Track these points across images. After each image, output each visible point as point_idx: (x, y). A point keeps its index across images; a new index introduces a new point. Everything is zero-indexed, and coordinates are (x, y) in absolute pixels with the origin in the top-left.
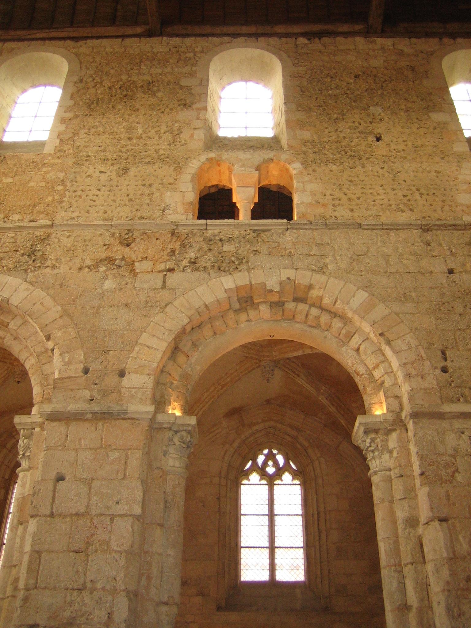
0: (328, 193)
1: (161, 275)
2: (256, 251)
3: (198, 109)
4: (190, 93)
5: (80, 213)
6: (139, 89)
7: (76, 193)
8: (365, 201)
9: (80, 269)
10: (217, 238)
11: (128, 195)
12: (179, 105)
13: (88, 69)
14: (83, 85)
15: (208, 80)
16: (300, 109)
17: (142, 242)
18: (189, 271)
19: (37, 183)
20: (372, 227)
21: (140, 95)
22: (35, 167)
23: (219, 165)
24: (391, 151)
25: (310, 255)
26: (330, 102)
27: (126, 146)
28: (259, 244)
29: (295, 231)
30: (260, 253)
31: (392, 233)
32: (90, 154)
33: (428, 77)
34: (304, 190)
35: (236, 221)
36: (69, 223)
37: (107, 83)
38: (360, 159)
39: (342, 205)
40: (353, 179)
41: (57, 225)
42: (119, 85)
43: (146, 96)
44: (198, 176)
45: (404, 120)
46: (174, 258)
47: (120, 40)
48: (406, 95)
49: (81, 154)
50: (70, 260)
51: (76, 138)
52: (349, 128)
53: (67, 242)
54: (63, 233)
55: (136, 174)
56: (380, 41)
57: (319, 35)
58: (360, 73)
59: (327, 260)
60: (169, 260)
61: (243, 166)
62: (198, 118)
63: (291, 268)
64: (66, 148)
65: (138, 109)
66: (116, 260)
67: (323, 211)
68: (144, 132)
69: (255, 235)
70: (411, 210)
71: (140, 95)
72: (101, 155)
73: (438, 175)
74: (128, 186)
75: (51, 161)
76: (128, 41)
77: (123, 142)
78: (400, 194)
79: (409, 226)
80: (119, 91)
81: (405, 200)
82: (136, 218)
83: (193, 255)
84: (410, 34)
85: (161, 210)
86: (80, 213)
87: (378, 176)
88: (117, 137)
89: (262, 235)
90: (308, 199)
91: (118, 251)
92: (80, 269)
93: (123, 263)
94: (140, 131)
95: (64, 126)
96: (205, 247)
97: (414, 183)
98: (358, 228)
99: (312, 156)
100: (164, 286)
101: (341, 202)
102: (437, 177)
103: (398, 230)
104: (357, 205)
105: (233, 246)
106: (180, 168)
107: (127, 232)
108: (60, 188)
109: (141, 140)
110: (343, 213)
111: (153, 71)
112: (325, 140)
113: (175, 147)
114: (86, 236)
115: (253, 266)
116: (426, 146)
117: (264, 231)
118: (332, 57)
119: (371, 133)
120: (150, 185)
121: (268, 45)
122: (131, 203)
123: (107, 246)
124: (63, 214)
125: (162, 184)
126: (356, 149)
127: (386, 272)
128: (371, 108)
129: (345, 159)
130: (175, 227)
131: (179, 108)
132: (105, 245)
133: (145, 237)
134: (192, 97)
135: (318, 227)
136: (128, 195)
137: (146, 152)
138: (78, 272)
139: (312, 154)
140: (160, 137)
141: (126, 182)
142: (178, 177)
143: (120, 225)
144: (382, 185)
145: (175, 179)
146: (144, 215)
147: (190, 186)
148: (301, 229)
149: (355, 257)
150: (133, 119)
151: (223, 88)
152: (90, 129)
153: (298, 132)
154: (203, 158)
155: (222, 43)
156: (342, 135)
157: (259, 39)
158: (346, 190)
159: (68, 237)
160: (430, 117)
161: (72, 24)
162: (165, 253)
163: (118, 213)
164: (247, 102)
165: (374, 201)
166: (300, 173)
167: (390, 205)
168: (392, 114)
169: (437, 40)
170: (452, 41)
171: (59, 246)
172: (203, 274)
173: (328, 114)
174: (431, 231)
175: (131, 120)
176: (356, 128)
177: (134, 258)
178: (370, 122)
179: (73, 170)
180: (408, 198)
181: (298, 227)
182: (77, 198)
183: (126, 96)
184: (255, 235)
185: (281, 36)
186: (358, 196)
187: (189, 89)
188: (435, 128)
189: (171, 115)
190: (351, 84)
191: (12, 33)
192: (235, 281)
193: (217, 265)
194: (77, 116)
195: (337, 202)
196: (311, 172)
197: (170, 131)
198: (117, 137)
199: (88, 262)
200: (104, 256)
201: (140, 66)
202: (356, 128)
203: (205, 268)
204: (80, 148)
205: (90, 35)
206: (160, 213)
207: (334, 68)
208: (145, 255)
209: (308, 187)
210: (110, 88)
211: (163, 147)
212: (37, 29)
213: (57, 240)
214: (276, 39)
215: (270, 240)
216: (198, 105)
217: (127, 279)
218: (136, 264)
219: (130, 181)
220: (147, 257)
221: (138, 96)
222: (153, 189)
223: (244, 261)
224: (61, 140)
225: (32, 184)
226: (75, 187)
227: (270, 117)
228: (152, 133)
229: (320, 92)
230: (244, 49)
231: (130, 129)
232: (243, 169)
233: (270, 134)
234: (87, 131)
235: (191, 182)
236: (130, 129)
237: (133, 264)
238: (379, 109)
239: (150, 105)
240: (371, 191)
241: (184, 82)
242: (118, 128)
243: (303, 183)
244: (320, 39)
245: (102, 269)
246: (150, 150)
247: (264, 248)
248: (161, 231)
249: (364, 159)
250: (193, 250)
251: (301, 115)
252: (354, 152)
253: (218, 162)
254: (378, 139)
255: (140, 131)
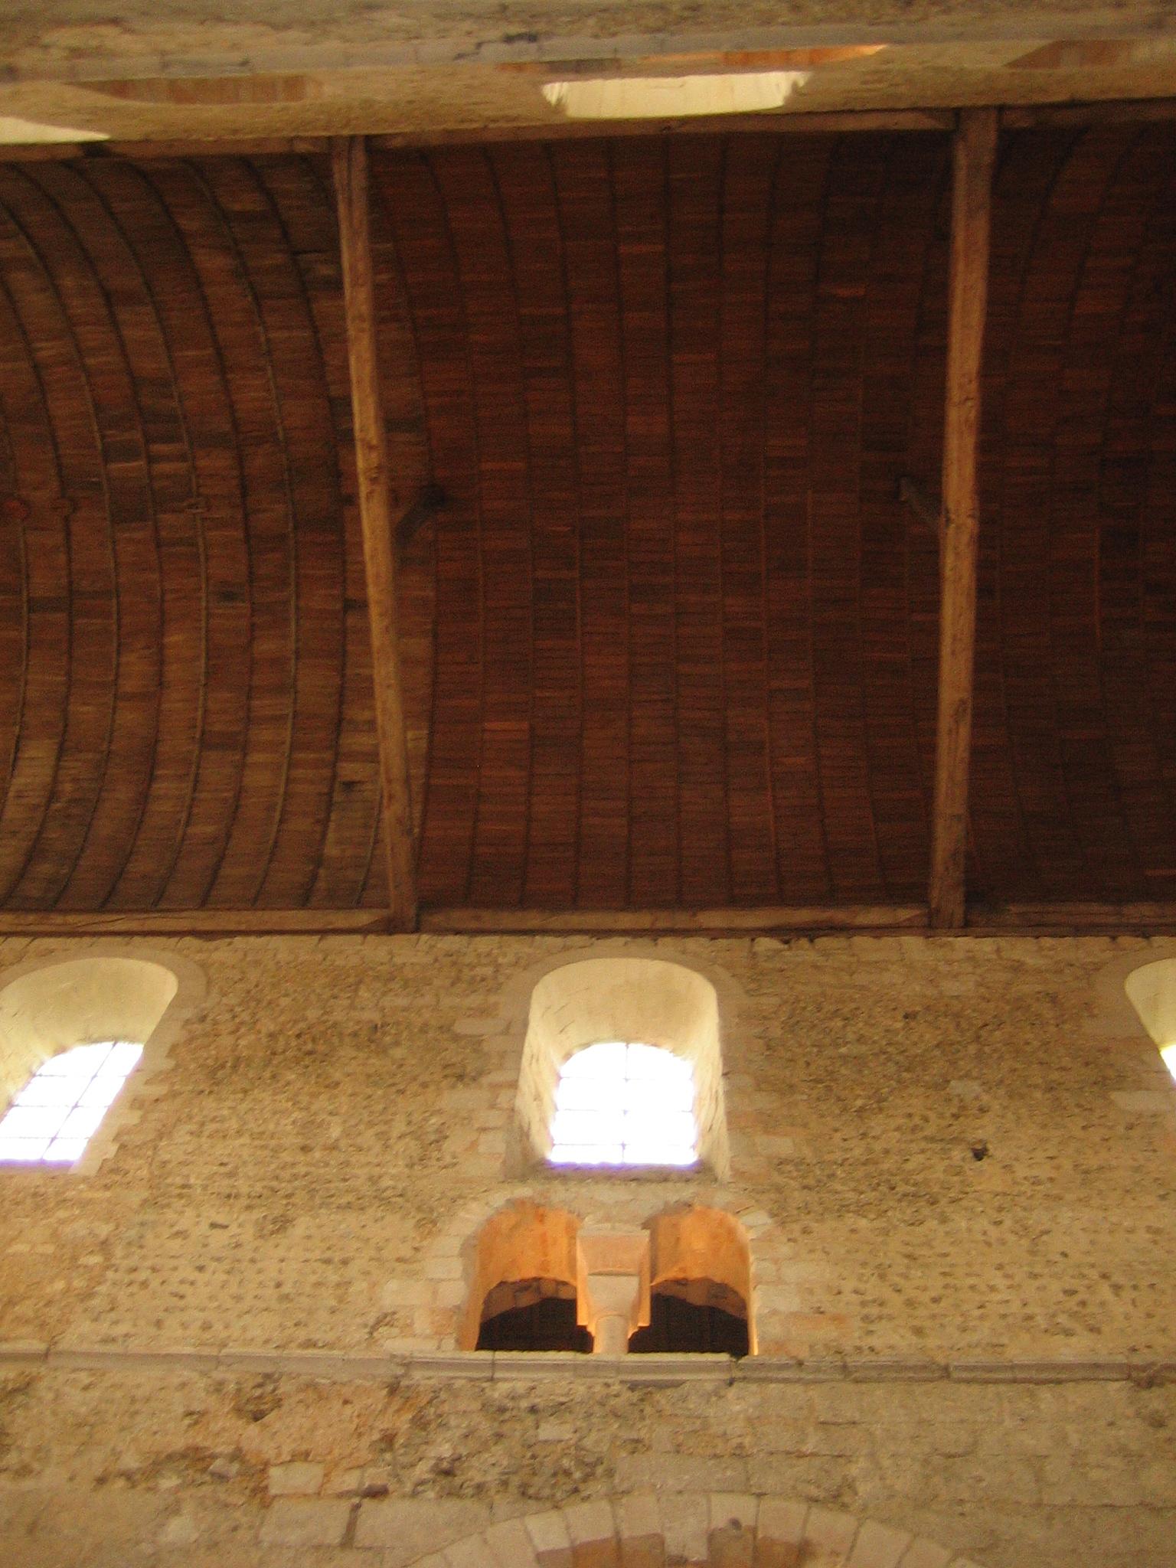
0: (848, 1285)
1: (345, 1506)
2: (637, 1441)
3: (495, 1087)
4: (475, 1051)
5: (135, 1325)
6: (347, 1040)
7: (133, 1276)
8: (957, 1306)
9: (101, 1481)
10: (524, 1404)
11: (279, 1285)
12: (446, 1077)
13: (225, 995)
14: (207, 1026)
15: (525, 1024)
16: (763, 1086)
17: (301, 1408)
18: (431, 1495)
19: (34, 1246)
20: (984, 1376)
21: (347, 1052)
22: (37, 1207)
23: (541, 1218)
24: (1015, 1183)
25: (801, 1456)
26: (843, 1071)
27: (293, 1164)
28: (648, 1422)
29: (754, 1387)
30: (649, 1448)
31: (1045, 1394)
32: (192, 1181)
33: (1093, 1016)
34: (779, 1281)
35: (581, 1357)
36: (99, 1348)
37: (267, 1025)
38: (933, 1202)
39: (891, 1318)
40: (918, 1252)
41: (60, 1354)
42: (296, 1030)
43: (361, 1055)
44: (482, 1246)
45: (1046, 1110)
46: (388, 1456)
47: (316, 938)
48: (1041, 1055)
49: (169, 1181)
50: (78, 1454)
51: (163, 1143)
52: (898, 1129)
53: (77, 1402)
54: (73, 1376)
55: (308, 1233)
56: (963, 944)
57: (811, 932)
58: (918, 1008)
59: (854, 1470)
60: (373, 1463)
61: (608, 1219)
62: (492, 1106)
63: (744, 1493)
64: (131, 1164)
65: (337, 1084)
66: (214, 1457)
67: (835, 1334)
68: (346, 1134)
69: (635, 1397)
70: (1093, 1330)
71: (347, 1052)
72: (224, 1185)
73: (1158, 1238)
74: (282, 1261)
75: (84, 1195)
76: (334, 941)
77: (286, 1157)
78: (1055, 1287)
79: (1093, 1372)
80: (294, 1043)
81: (1072, 1303)
82: (292, 1345)
83: (445, 1450)
84: (1036, 928)
85: (366, 1326)
86: (135, 1325)
87: (989, 1244)
88: (273, 1143)
89: (658, 1396)
90: (789, 1303)
91: (227, 1432)
92: (101, 1481)
93: (235, 1467)
94: (335, 1132)
95: (139, 1113)
96: (486, 1428)
97: (1091, 1259)
98: (941, 1378)
99: (798, 1197)
100: (348, 1541)
101: (886, 1311)
102: (1155, 1242)
103: (1059, 1382)
104: (934, 1317)
105: (568, 1426)
106: (434, 1222)
107: (260, 1380)
108: (95, 1260)
109: (335, 1153)
110: (893, 1340)
111: (388, 1001)
112: (832, 1157)
113: (426, 1172)
114: (139, 1386)
115: (625, 1486)
116: (1111, 1169)
117: (662, 1386)
118: (846, 978)
119: (956, 1140)
120: (345, 1262)
121: (683, 953)
122: (284, 1306)
123: (196, 1417)
124: (86, 1326)
125: (378, 1260)
126: (920, 1178)
127: (1039, 1505)
128: (953, 1083)
129: (891, 1203)
130: (400, 1371)
131: (444, 1083)
132: (191, 1414)
133: (311, 1395)
134: (481, 1059)
135: (821, 1376)
136: (279, 1285)
137: (345, 1180)
138: (95, 1490)
139: (796, 1193)
140: (386, 1147)
141: (281, 1252)
142: (425, 1243)
143: (242, 1359)
144: (1000, 1267)
145: (416, 1249)
146: (316, 1336)
147: (456, 1267)
148: (771, 1381)
149: (936, 1460)
150: (322, 1103)
151: (568, 1056)
152: (203, 1124)
153: (761, 1139)
154: (499, 1199)
155: (566, 948)
156: (878, 1146)
157: (661, 941)
158: (897, 1279)
159: (86, 1388)
160: (1112, 1103)
161: (203, 902)
162: (365, 1442)
163: (244, 1329)
164: (626, 1081)
165: (980, 1307)
166: (767, 1238)
167: (1030, 1318)
168: (1011, 1097)
169: (1104, 941)
170: (1141, 942)
171: (54, 1413)
172: (474, 1507)
173: (839, 1099)
174: (1161, 1385)
175: (314, 1108)
176: (914, 1129)
177: (269, 1453)
178: (953, 1115)
179: (138, 1219)
180: (1077, 1298)
181: (763, 1374)
182: (134, 1288)
183: (310, 1053)
184: (635, 1397)
185: (714, 934)
186: (933, 1294)
187: (476, 1043)
188: (1130, 1127)
189: (420, 1098)
190: (896, 1032)
191: (58, 919)
192: (568, 1528)
193: (515, 1480)
194: (174, 1095)
195: (874, 1311)
196: (796, 1234)
197: (417, 1135)
198: (273, 1143)
199: (131, 1461)
200: (179, 1444)
201: (356, 991)
202: (914, 1129)
203: (480, 1488)
204: (169, 1166)
205: (243, 927)
206: (363, 1334)
207: (852, 1000)
208: (304, 1447)
209: (791, 1272)
210: (272, 1036)
211: (394, 1171)
212: (119, 911)
213: (50, 1396)
214: (703, 941)
215: (679, 1412)
216: (496, 1077)
217: (238, 1514)
218: (274, 1472)
219: (289, 1249)
220: (307, 1454)
221: (342, 1053)
222: (353, 1270)
223: (600, 1470)
224: (123, 1147)
225: (20, 1247)
226: (133, 1262)
227: (691, 1118)
228: (368, 1137)
229: (815, 1050)
230: (624, 961)
231: (309, 1126)
232: (608, 1225)
233: (683, 1154)
234: (193, 1127)
235: (461, 1255)
236: (309, 1126)
237: (263, 1471)
238: (975, 1087)
239: (369, 1076)
240: (971, 1281)
241: (465, 1027)
242: (278, 1124)
243: (776, 1261)
244: (812, 941)
245: (169, 1482)
246: (357, 1177)
247: (661, 1434)
248: (358, 1382)
249: (943, 1201)
250: (449, 1434)
251: (764, 1101)
252: (915, 1184)
253: (538, 1211)
254: (979, 1155)
255: (335, 1132)
